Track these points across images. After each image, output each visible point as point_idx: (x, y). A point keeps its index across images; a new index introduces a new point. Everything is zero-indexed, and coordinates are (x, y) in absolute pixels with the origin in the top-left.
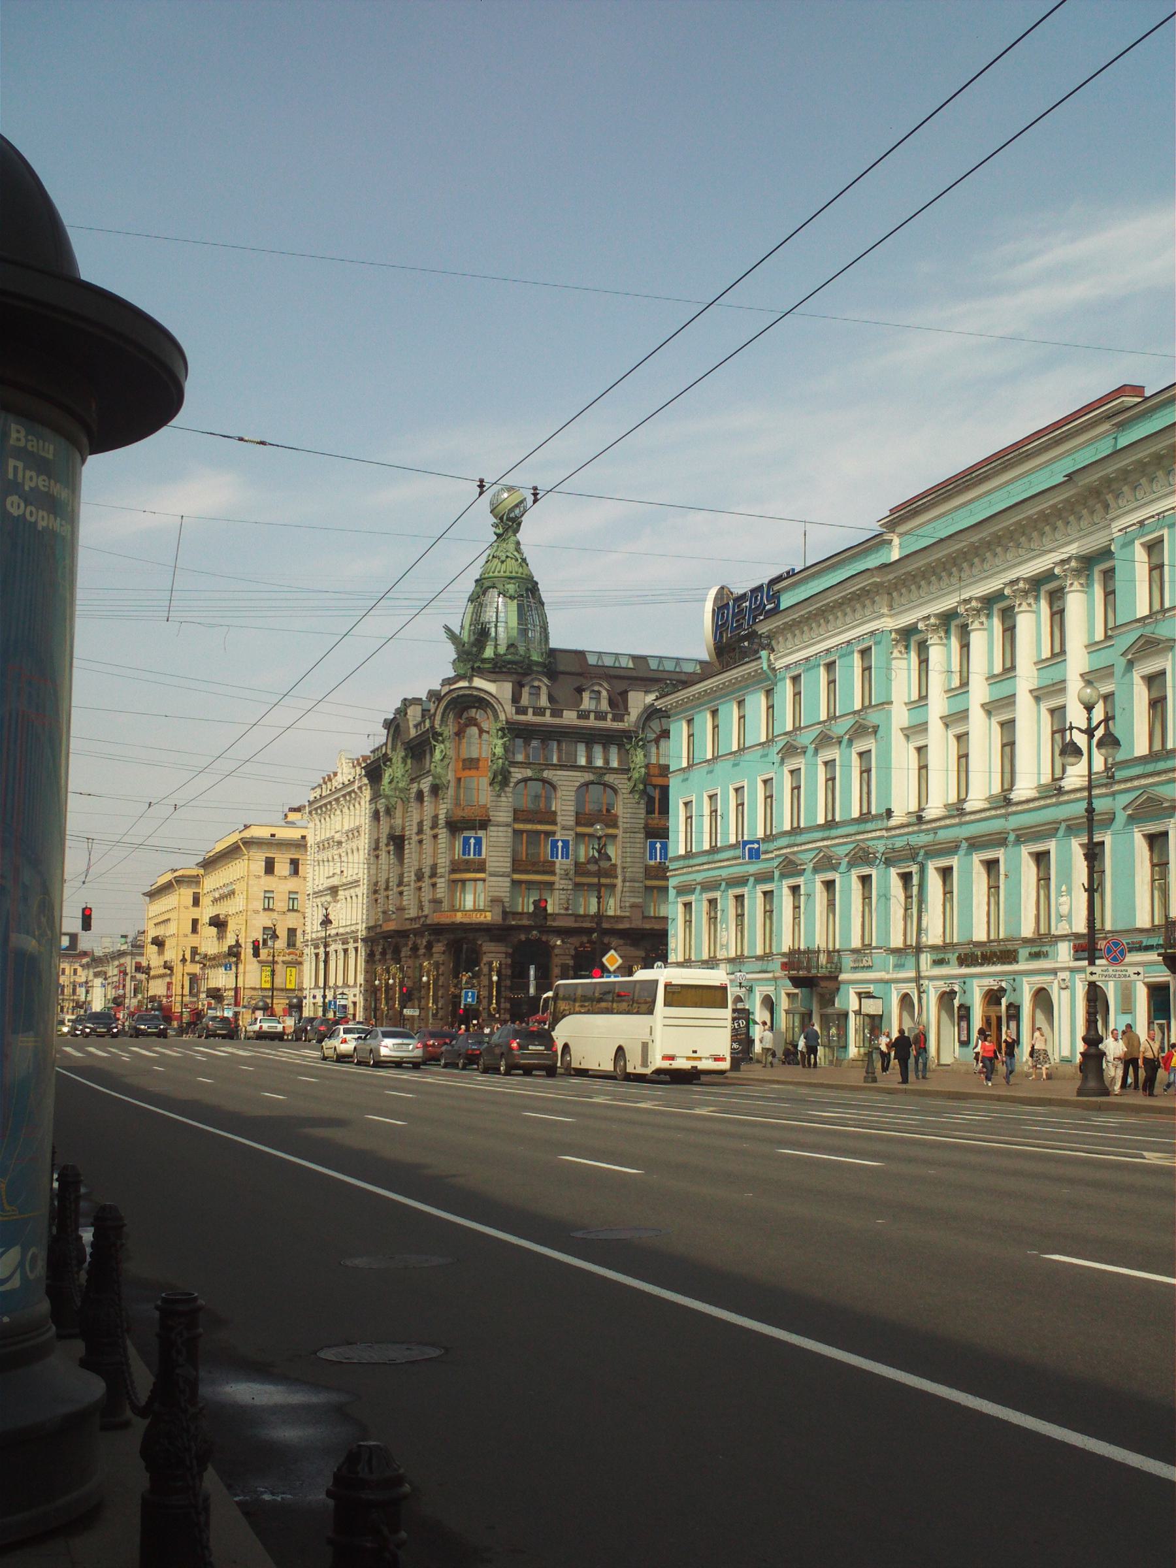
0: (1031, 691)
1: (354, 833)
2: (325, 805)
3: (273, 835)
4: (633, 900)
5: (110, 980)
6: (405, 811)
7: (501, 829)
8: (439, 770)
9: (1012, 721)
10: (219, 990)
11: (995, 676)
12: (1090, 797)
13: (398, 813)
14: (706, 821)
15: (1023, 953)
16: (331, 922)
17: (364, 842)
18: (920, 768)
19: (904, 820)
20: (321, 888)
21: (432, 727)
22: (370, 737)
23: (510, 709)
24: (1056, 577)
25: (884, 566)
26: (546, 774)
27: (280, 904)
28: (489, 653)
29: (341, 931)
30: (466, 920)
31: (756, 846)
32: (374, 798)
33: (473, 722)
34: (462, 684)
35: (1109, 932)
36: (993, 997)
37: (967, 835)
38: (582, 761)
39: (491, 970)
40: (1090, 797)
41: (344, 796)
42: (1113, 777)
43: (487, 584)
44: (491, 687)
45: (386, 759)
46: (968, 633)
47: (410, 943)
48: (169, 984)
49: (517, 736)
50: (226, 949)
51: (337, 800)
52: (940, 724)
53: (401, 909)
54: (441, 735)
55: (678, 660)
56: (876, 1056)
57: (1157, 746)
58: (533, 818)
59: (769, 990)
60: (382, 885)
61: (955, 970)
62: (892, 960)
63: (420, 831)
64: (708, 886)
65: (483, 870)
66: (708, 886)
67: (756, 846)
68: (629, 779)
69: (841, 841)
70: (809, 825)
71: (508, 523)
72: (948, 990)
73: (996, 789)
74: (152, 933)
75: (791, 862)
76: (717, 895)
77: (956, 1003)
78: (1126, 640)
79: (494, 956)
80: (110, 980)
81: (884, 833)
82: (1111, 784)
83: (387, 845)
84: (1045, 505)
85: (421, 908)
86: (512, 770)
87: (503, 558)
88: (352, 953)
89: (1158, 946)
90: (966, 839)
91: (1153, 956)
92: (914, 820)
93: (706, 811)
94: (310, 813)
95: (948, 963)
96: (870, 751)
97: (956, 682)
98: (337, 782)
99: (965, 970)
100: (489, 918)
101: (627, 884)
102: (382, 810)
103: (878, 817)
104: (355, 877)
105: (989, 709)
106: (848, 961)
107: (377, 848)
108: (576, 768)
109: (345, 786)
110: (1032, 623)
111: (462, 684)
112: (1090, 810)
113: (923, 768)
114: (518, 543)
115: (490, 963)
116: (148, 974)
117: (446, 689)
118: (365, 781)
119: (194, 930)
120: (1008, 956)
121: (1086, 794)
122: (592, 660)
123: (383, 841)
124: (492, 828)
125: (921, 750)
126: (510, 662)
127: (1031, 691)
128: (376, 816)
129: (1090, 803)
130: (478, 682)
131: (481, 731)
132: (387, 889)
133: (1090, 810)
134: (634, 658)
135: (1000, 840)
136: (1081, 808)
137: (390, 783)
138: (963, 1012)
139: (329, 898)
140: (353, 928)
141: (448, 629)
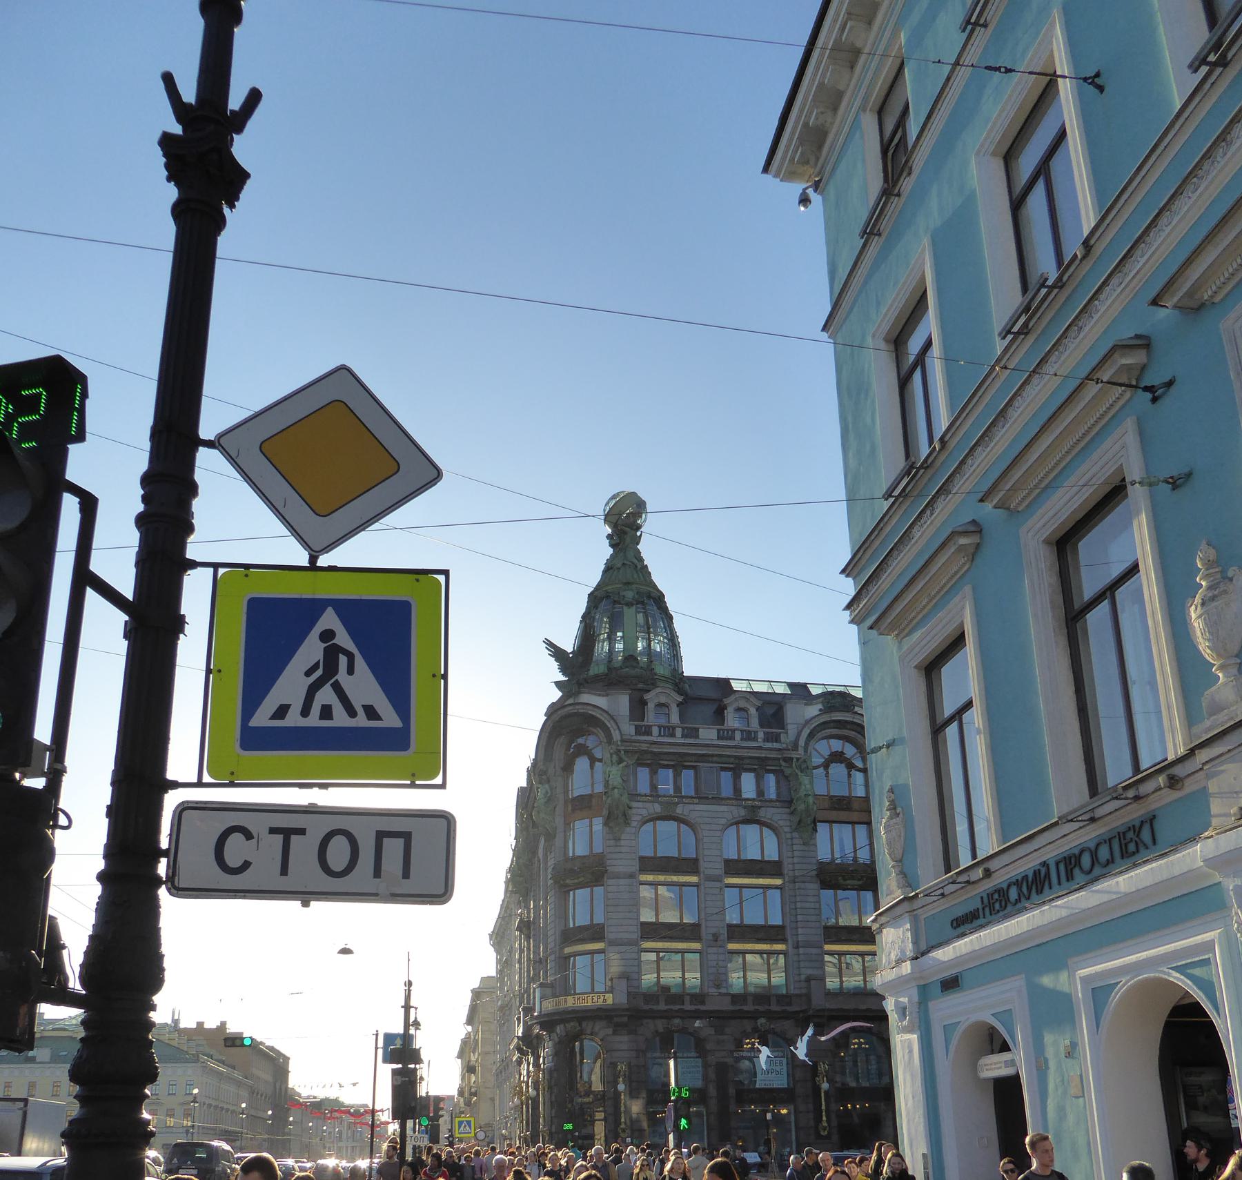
4: (810, 972)
7: (622, 882)
23: (629, 729)
26: (679, 810)
30: (581, 1005)
33: (583, 751)
44: (601, 701)
49: (640, 764)
56: (859, 764)
86: (634, 804)
100: (610, 1001)
108: (718, 800)
124: (611, 882)
131: (593, 760)
141: (549, 644)
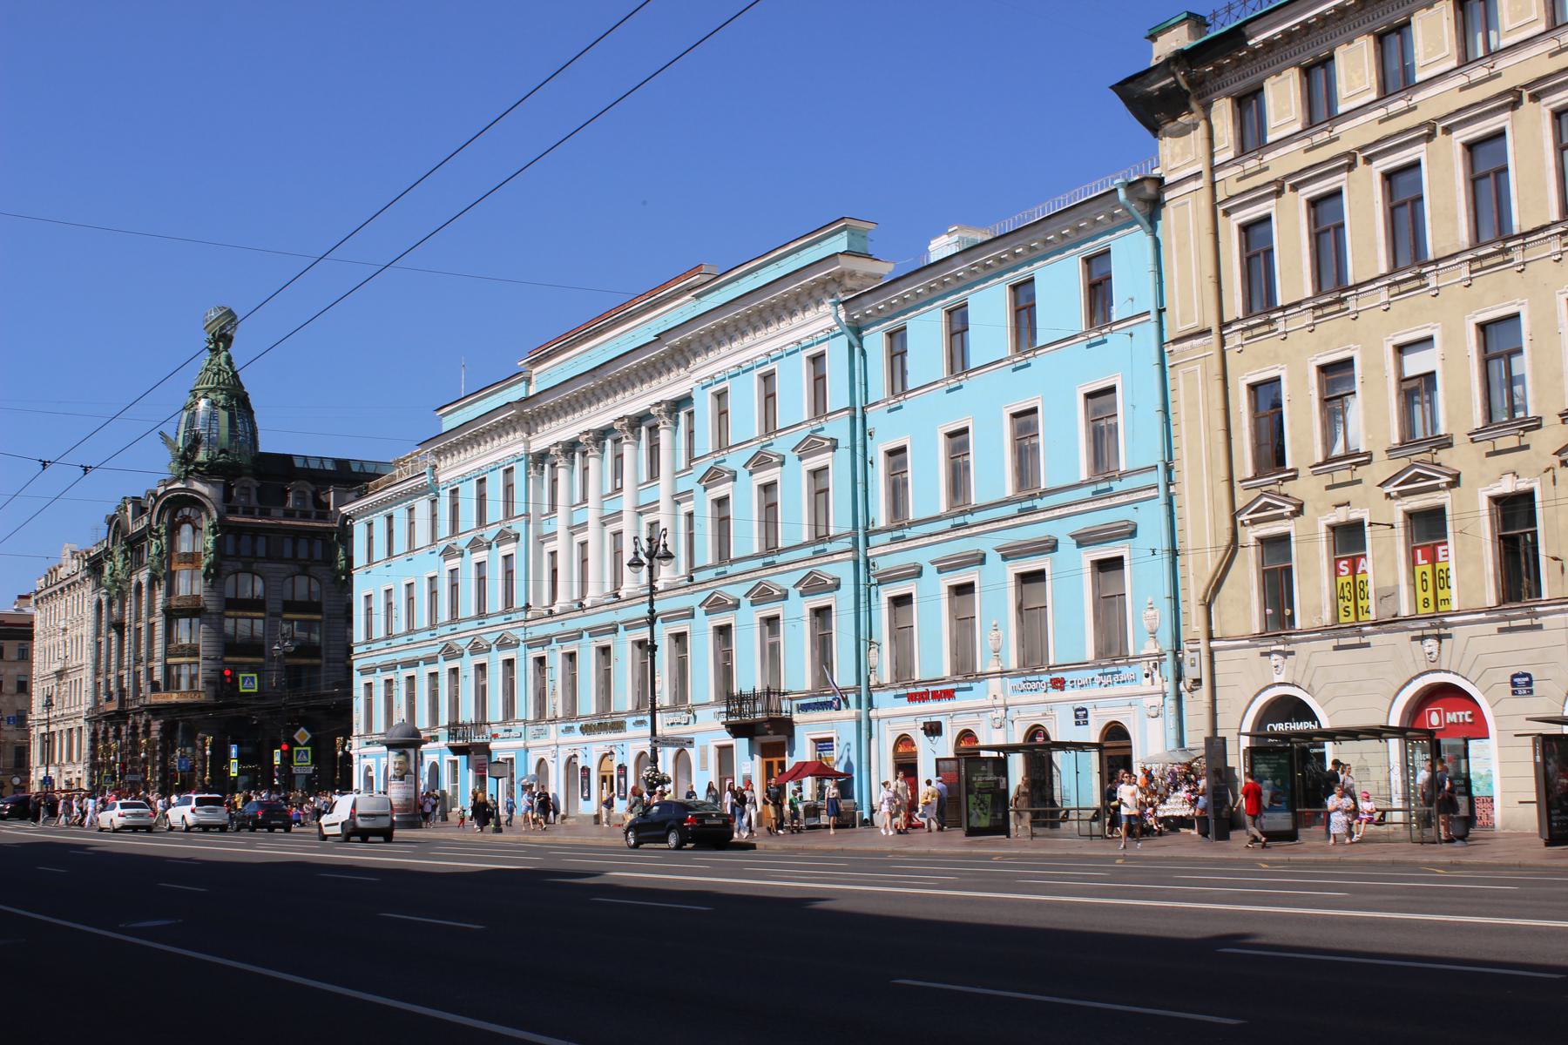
22: (93, 537)
34: (178, 485)
38: (288, 553)
55: (362, 463)
57: (772, 545)
64: (386, 668)
66: (386, 668)
69: (926, 541)
71: (222, 339)
92: (576, 606)
96: (1517, 316)
98: (63, 573)
99: (586, 738)
108: (281, 560)
109: (69, 576)
111: (178, 485)
112: (652, 611)
117: (161, 490)
120: (618, 726)
122: (298, 464)
133: (652, 611)
134: (337, 462)
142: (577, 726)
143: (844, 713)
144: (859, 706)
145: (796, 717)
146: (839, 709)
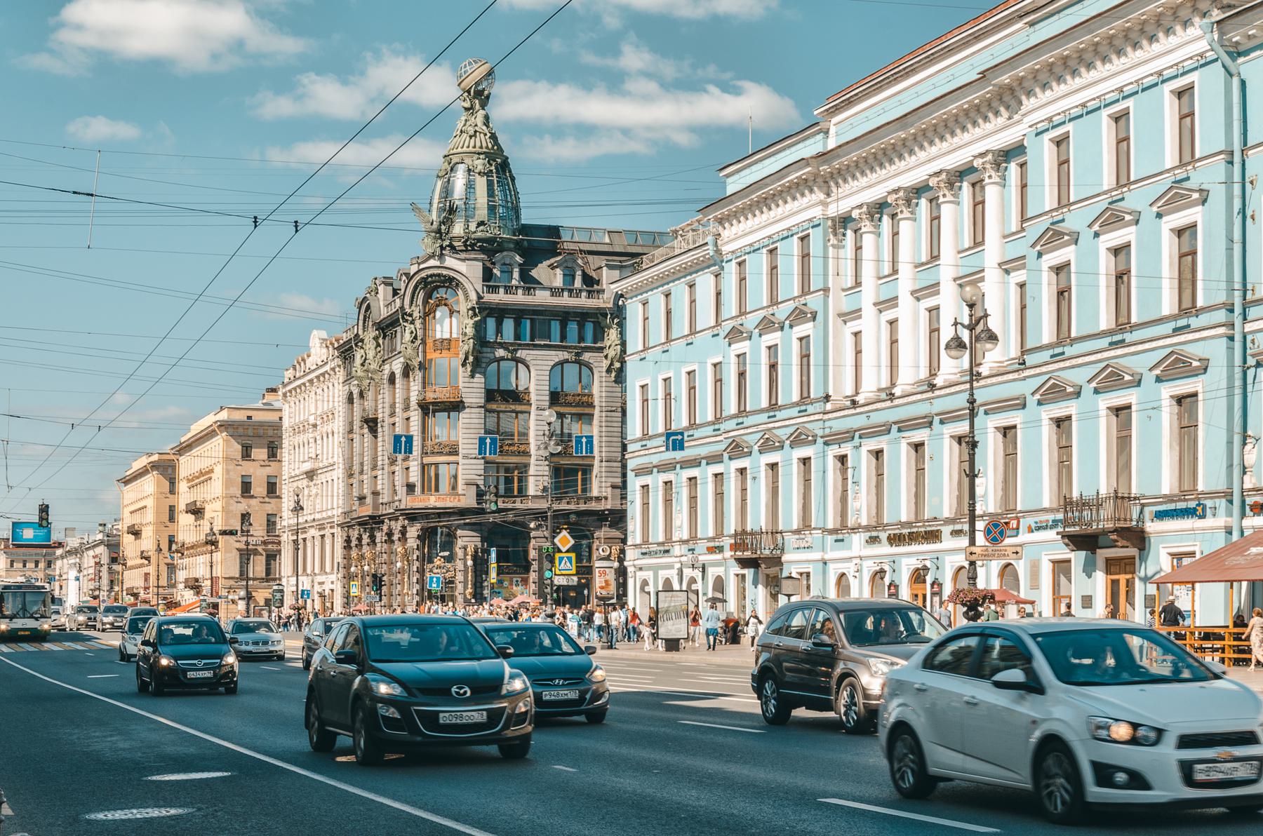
0: (955, 280)
1: (328, 416)
2: (299, 387)
3: (249, 418)
5: (85, 572)
6: (377, 393)
8: (409, 351)
9: (937, 308)
10: (197, 580)
11: (923, 264)
12: (972, 388)
13: (370, 395)
14: (661, 403)
15: (946, 530)
16: (302, 509)
17: (339, 425)
18: (932, 331)
19: (909, 389)
20: (297, 472)
21: (402, 308)
24: (976, 170)
25: (822, 156)
27: (259, 489)
28: (458, 229)
29: (318, 516)
31: (680, 437)
32: (349, 377)
33: (442, 302)
34: (432, 263)
35: (1021, 512)
36: (918, 576)
37: (896, 419)
39: (466, 554)
40: (972, 388)
41: (318, 377)
42: (1024, 363)
43: (455, 159)
44: (462, 267)
45: (358, 340)
46: (938, 206)
47: (385, 528)
48: (147, 575)
50: (203, 537)
51: (311, 381)
52: (874, 310)
53: (376, 493)
54: (411, 315)
58: (503, 398)
59: (720, 571)
60: (356, 468)
61: (885, 549)
62: (830, 539)
63: (392, 414)
65: (456, 453)
67: (680, 437)
68: (606, 357)
70: (1080, 335)
72: (878, 568)
73: (924, 373)
74: (128, 520)
75: (737, 446)
76: (846, 449)
77: (887, 581)
78: (1036, 229)
79: (467, 541)
80: (85, 572)
81: (820, 416)
82: (891, 400)
83: (361, 428)
84: (964, 102)
85: (395, 492)
87: (472, 133)
88: (328, 541)
89: (1055, 523)
90: (895, 423)
91: (1051, 535)
92: (883, 396)
93: (661, 395)
94: (285, 395)
95: (880, 542)
97: (887, 269)
99: (895, 550)
101: (604, 464)
102: (356, 391)
103: (817, 400)
104: (331, 461)
105: (917, 295)
106: (791, 540)
107: (351, 431)
110: (955, 214)
111: (432, 263)
112: (972, 401)
113: (894, 342)
114: (487, 118)
115: (465, 548)
116: (124, 564)
118: (338, 361)
119: (172, 519)
120: (933, 536)
121: (968, 386)
123: (357, 424)
125: (893, 323)
126: (479, 240)
127: (955, 280)
128: (350, 400)
129: (972, 395)
130: (450, 261)
132: (361, 472)
133: (972, 401)
135: (927, 422)
136: (961, 401)
137: (362, 365)
138: (893, 590)
139: (305, 482)
140: (330, 513)
142: (883, 536)
143: (1209, 522)
144: (1230, 514)
145: (1151, 527)
146: (1203, 517)
